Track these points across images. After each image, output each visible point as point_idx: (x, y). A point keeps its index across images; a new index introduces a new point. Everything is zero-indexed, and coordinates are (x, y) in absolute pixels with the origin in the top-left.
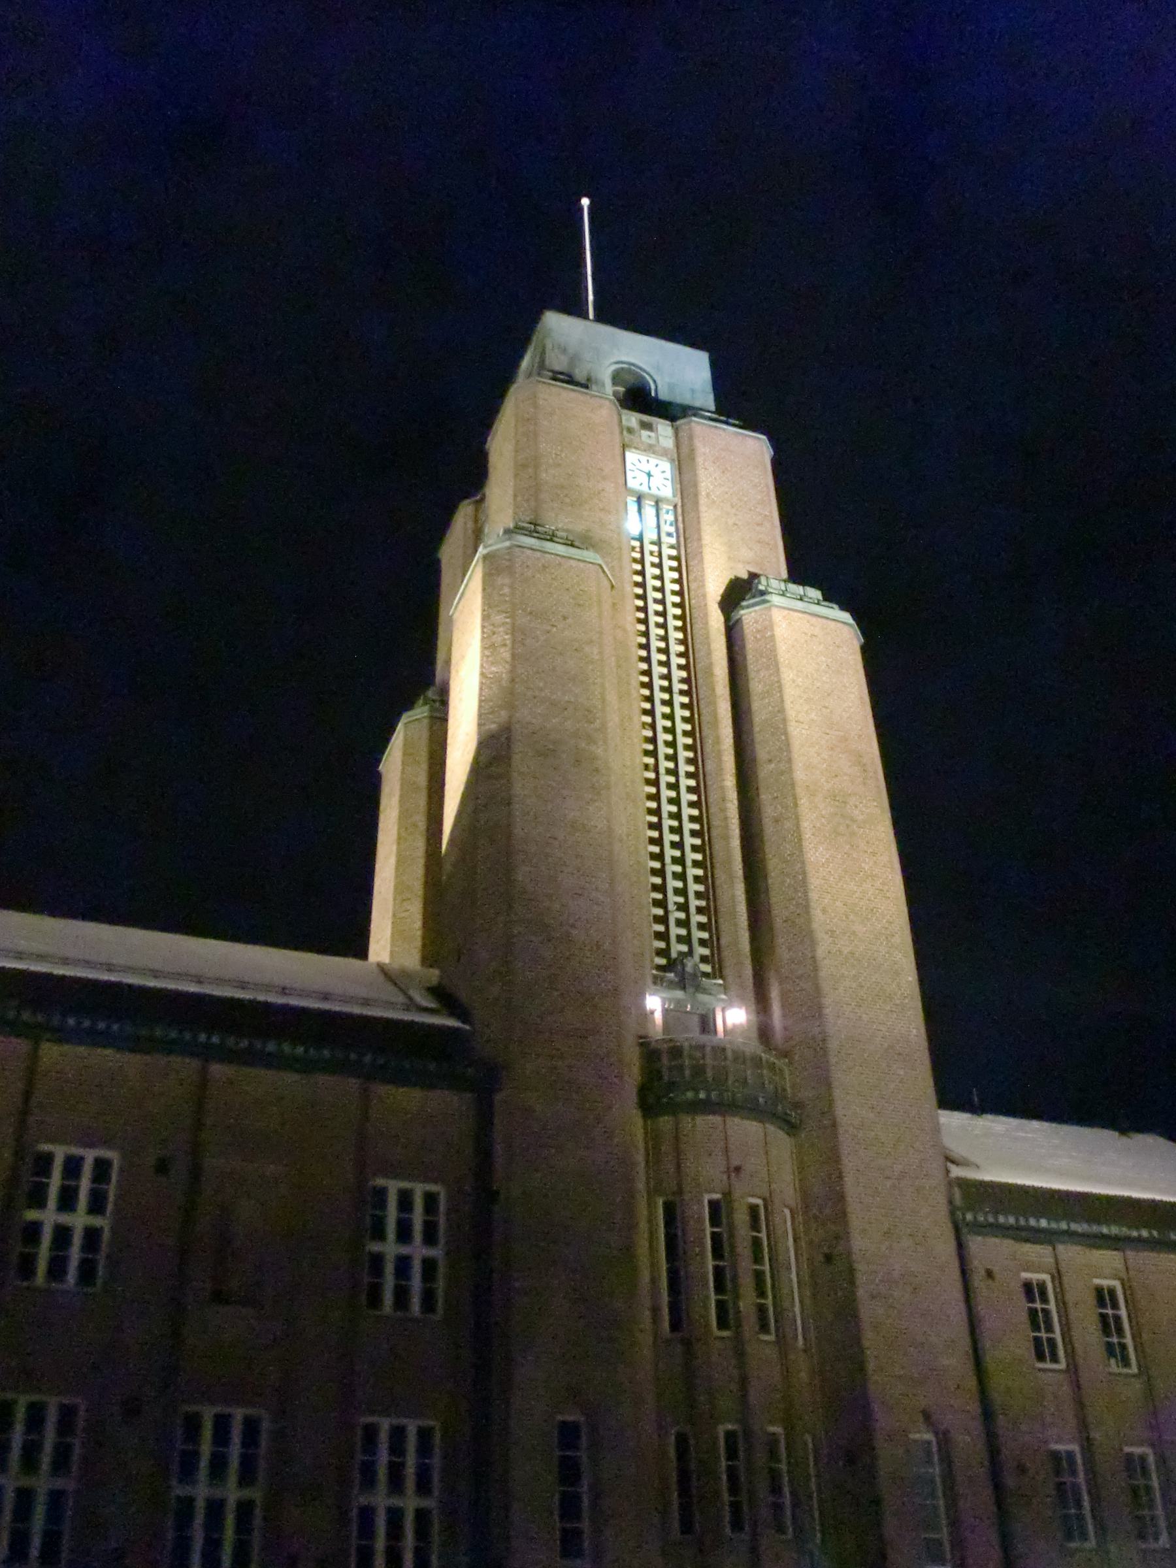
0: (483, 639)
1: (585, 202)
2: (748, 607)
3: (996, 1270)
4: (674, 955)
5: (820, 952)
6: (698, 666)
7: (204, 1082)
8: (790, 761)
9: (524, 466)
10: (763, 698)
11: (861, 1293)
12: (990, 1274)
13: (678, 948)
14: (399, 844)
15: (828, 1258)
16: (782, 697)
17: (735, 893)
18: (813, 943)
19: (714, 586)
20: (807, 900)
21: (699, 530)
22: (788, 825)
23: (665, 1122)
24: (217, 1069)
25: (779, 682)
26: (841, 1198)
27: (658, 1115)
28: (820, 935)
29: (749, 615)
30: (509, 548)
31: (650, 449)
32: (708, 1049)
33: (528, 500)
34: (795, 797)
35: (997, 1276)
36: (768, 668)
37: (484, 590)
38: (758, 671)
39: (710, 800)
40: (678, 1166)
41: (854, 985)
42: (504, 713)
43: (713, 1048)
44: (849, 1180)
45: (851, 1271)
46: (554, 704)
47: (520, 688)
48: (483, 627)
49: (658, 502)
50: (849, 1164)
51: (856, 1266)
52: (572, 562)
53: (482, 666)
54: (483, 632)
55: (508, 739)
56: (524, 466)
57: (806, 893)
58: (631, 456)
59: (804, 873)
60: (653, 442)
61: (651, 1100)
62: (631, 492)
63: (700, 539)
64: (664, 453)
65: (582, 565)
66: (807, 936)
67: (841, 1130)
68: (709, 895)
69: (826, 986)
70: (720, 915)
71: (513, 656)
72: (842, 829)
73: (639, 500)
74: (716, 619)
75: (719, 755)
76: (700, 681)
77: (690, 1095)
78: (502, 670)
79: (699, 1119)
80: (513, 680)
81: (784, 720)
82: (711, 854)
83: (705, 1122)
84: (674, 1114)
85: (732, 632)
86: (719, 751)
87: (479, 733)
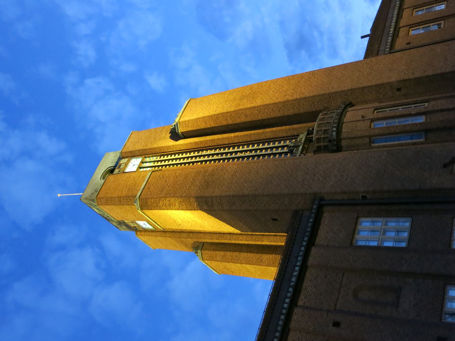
0: (167, 209)
1: (59, 195)
2: (178, 130)
3: (408, 42)
4: (287, 151)
5: (290, 98)
6: (194, 147)
7: (304, 307)
8: (227, 113)
9: (120, 202)
10: (207, 123)
11: (411, 77)
12: (408, 44)
13: (286, 150)
14: (242, 263)
15: (399, 90)
16: (207, 117)
17: (268, 132)
18: (288, 101)
19: (172, 143)
20: (273, 104)
21: (153, 149)
22: (248, 112)
23: (344, 143)
24: (300, 303)
25: (202, 118)
26: (377, 85)
27: (341, 147)
28: (285, 99)
29: (180, 130)
30: (139, 200)
31: (126, 165)
32: (318, 129)
33: (130, 200)
34: (239, 110)
35: (409, 42)
36: (197, 122)
37: (151, 209)
38: (198, 126)
39: (238, 142)
40: (360, 137)
41: (304, 88)
42: (192, 200)
43: (318, 127)
44: (370, 84)
45: (404, 81)
46: (192, 183)
47: (185, 195)
48: (163, 209)
49: (142, 162)
50: (365, 84)
51: (402, 79)
52: (149, 180)
53: (176, 209)
54: (165, 209)
55: (201, 197)
56: (120, 202)
57: (270, 104)
58: (127, 170)
59: (264, 106)
60: (124, 164)
61: (334, 148)
62: (137, 170)
63: (156, 148)
64: (129, 161)
65: (151, 177)
66: (285, 103)
67: (353, 88)
68: (268, 141)
69: (303, 96)
70: (276, 137)
71: (173, 197)
72: (252, 96)
73: (140, 168)
74: (181, 142)
75: (223, 139)
76: (199, 147)
77: (334, 134)
78: (177, 201)
79: (344, 130)
80: (181, 197)
81: (214, 115)
82: (255, 141)
83: (345, 129)
84: (341, 139)
85: (186, 136)
86: (222, 139)
87: (197, 210)
